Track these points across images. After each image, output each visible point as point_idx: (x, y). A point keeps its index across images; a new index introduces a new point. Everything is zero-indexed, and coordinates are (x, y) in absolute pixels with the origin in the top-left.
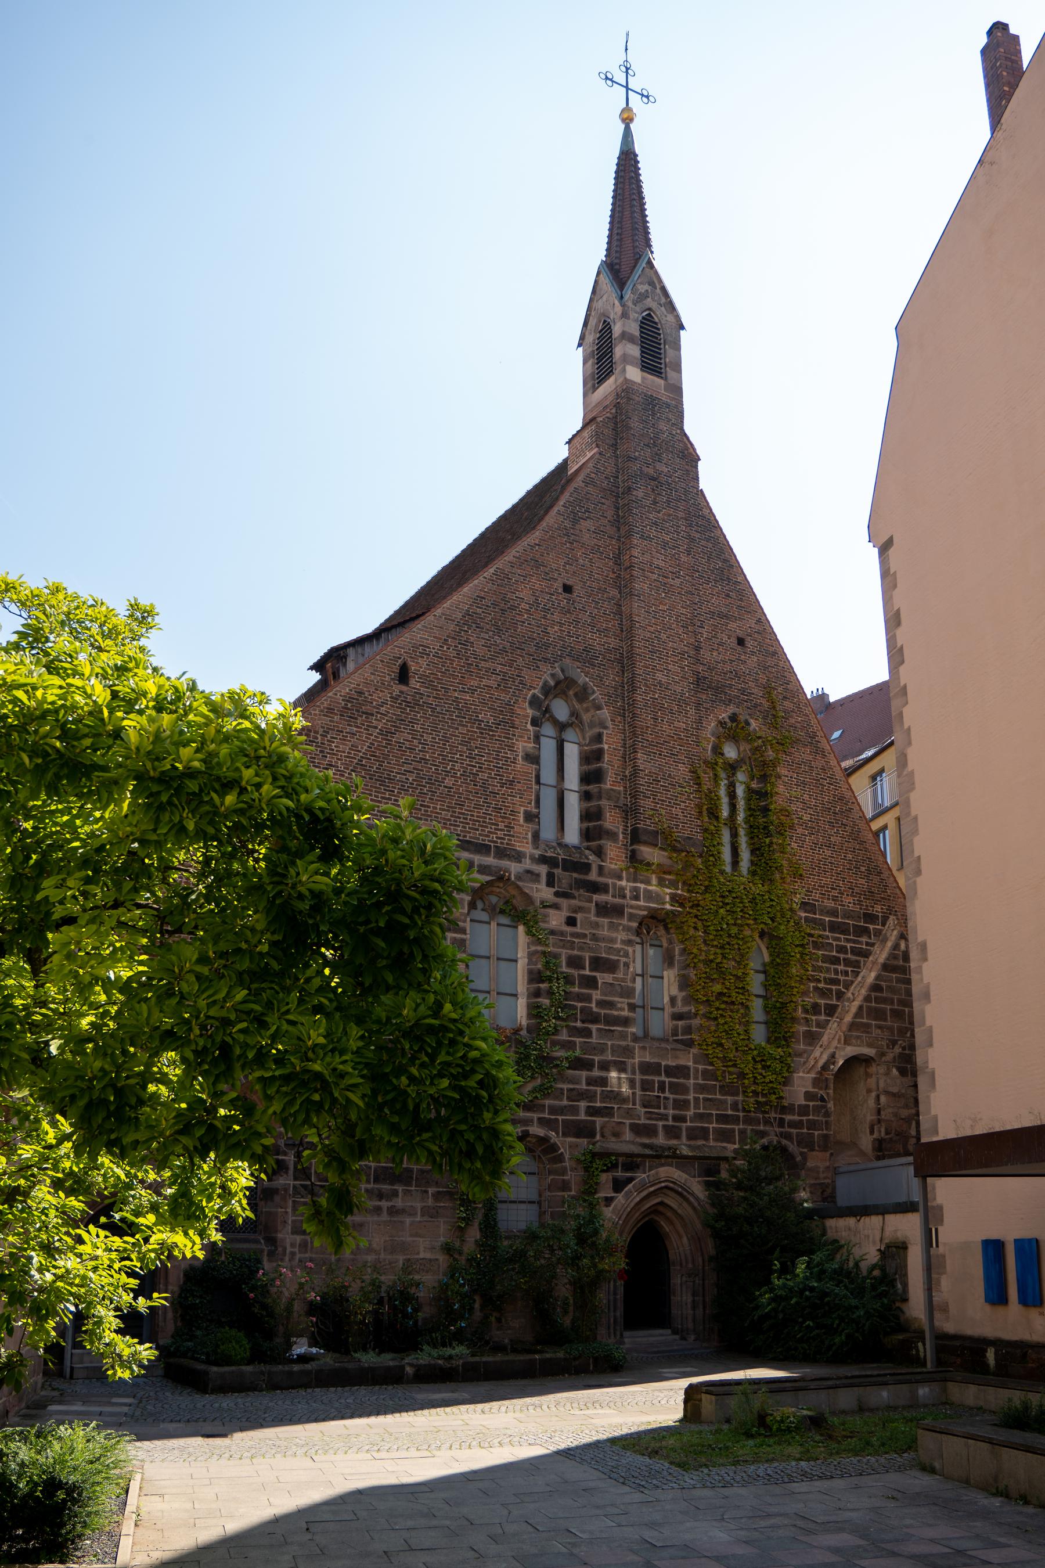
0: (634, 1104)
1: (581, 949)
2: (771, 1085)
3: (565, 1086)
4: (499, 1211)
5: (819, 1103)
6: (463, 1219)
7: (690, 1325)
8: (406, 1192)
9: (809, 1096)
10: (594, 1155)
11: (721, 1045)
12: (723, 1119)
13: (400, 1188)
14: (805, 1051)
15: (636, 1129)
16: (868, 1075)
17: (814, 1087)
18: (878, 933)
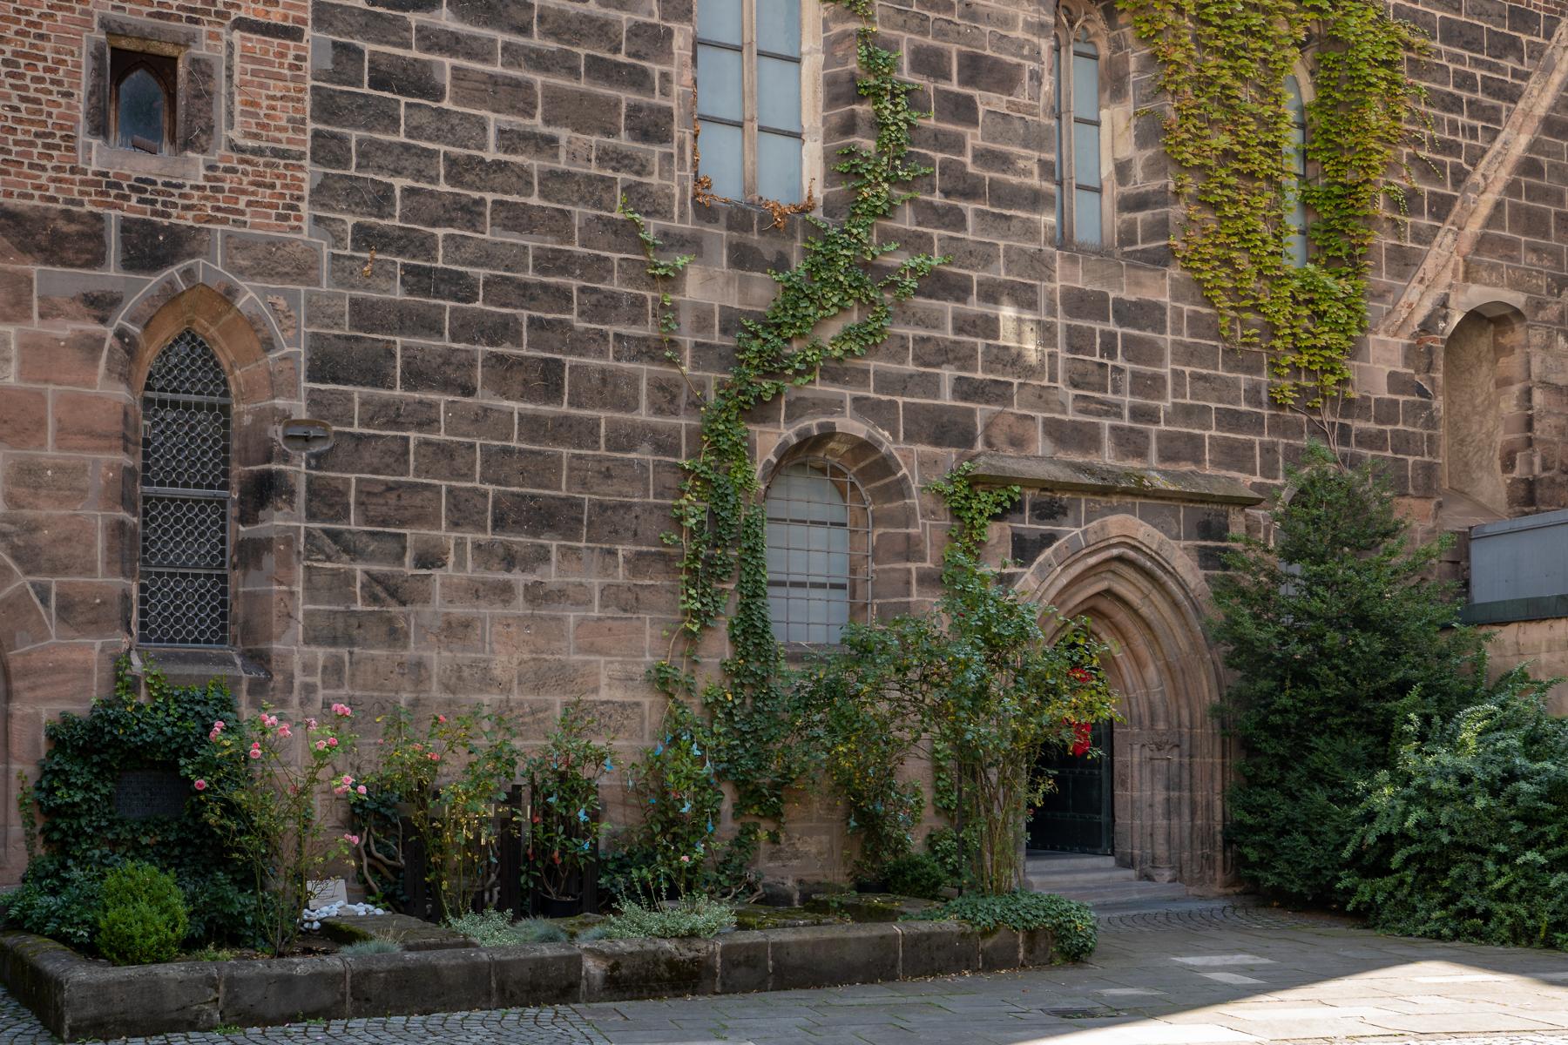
0: (1053, 378)
1: (941, 34)
2: (1327, 353)
3: (911, 332)
4: (769, 601)
5: (1416, 398)
6: (695, 614)
7: (1161, 850)
8: (566, 552)
9: (1395, 382)
10: (974, 481)
11: (1228, 262)
12: (1231, 419)
13: (553, 543)
14: (1390, 289)
15: (1060, 433)
16: (1499, 350)
17: (1407, 365)
18: (1537, 52)
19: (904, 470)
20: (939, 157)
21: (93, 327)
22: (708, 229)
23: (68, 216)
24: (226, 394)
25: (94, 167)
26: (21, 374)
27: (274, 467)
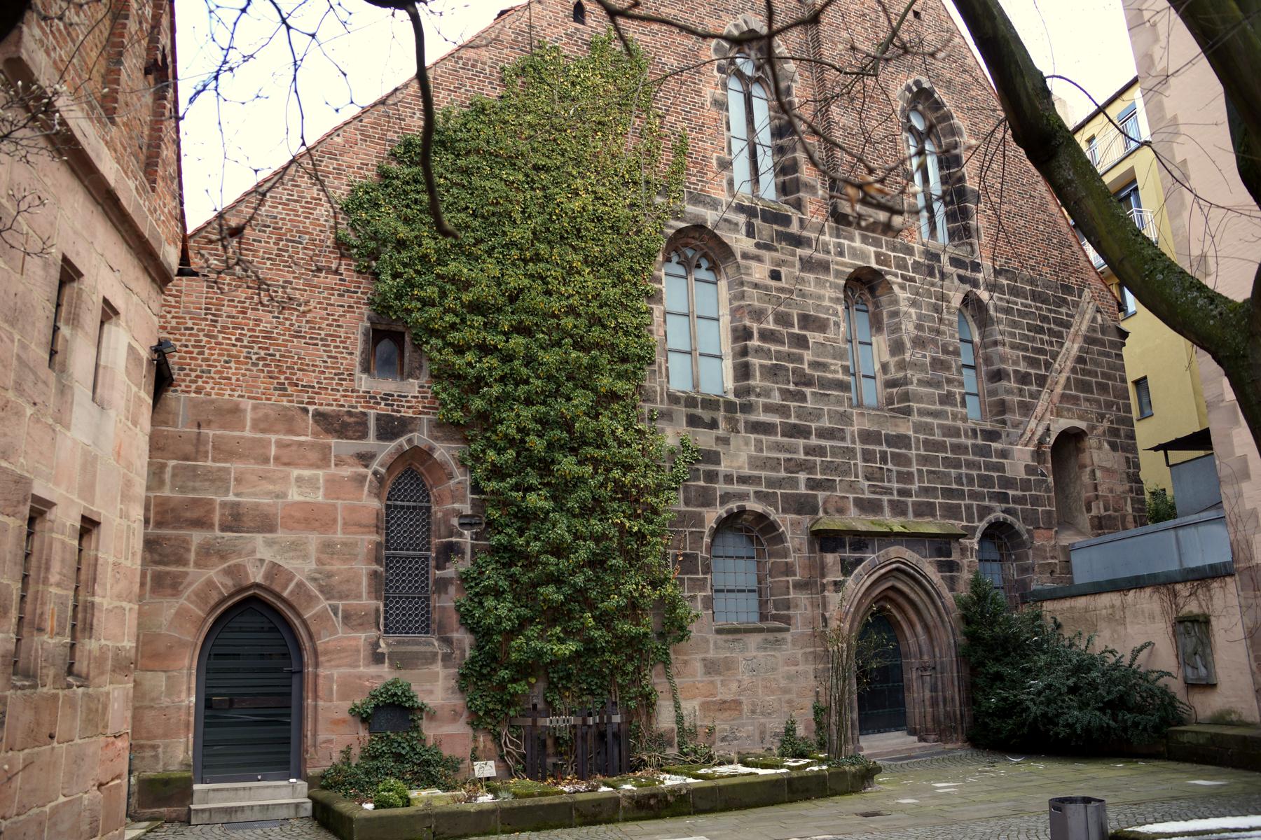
0: (856, 476)
12: (948, 493)
14: (1021, 423)
20: (791, 366)
21: (362, 470)
22: (675, 407)
23: (349, 414)
24: (428, 501)
25: (363, 389)
26: (326, 496)
27: (454, 539)
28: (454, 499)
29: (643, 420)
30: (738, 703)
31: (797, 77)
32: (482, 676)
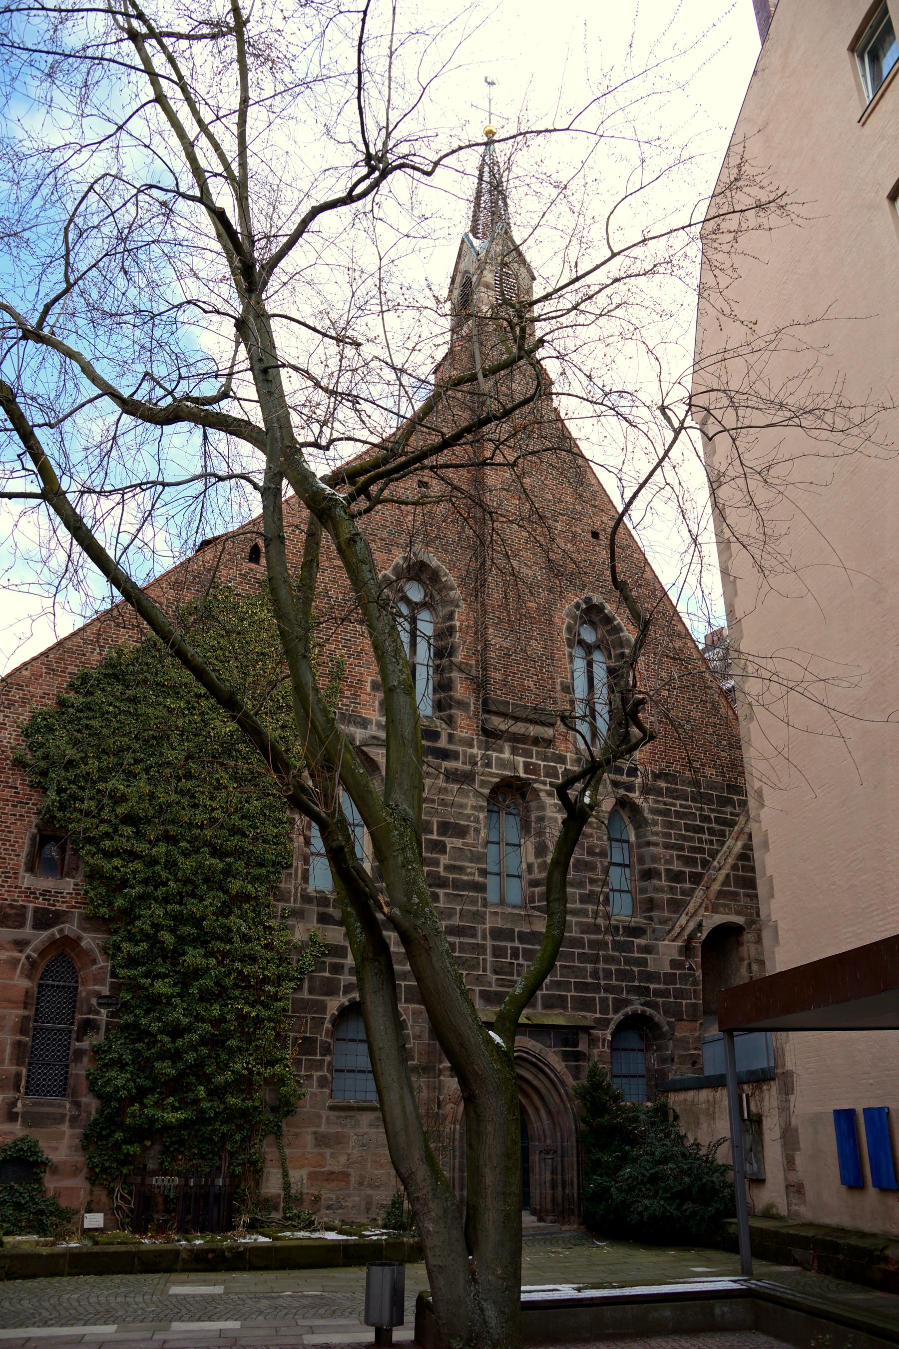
0: (485, 970)
14: (670, 919)
19: (404, 1017)
21: (16, 954)
22: (307, 906)
24: (77, 982)
27: (91, 1017)
28: (96, 983)
29: (275, 917)
30: (345, 1176)
31: (461, 603)
32: (101, 1137)
